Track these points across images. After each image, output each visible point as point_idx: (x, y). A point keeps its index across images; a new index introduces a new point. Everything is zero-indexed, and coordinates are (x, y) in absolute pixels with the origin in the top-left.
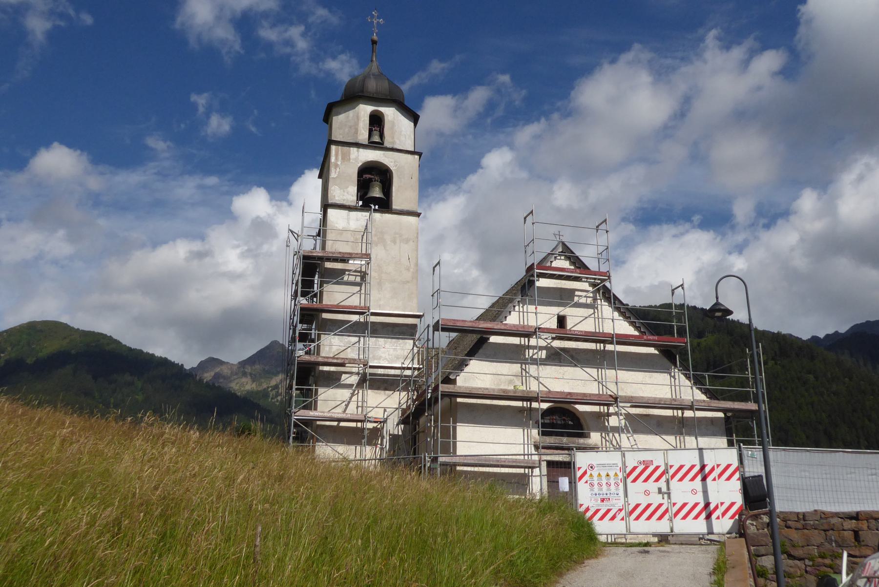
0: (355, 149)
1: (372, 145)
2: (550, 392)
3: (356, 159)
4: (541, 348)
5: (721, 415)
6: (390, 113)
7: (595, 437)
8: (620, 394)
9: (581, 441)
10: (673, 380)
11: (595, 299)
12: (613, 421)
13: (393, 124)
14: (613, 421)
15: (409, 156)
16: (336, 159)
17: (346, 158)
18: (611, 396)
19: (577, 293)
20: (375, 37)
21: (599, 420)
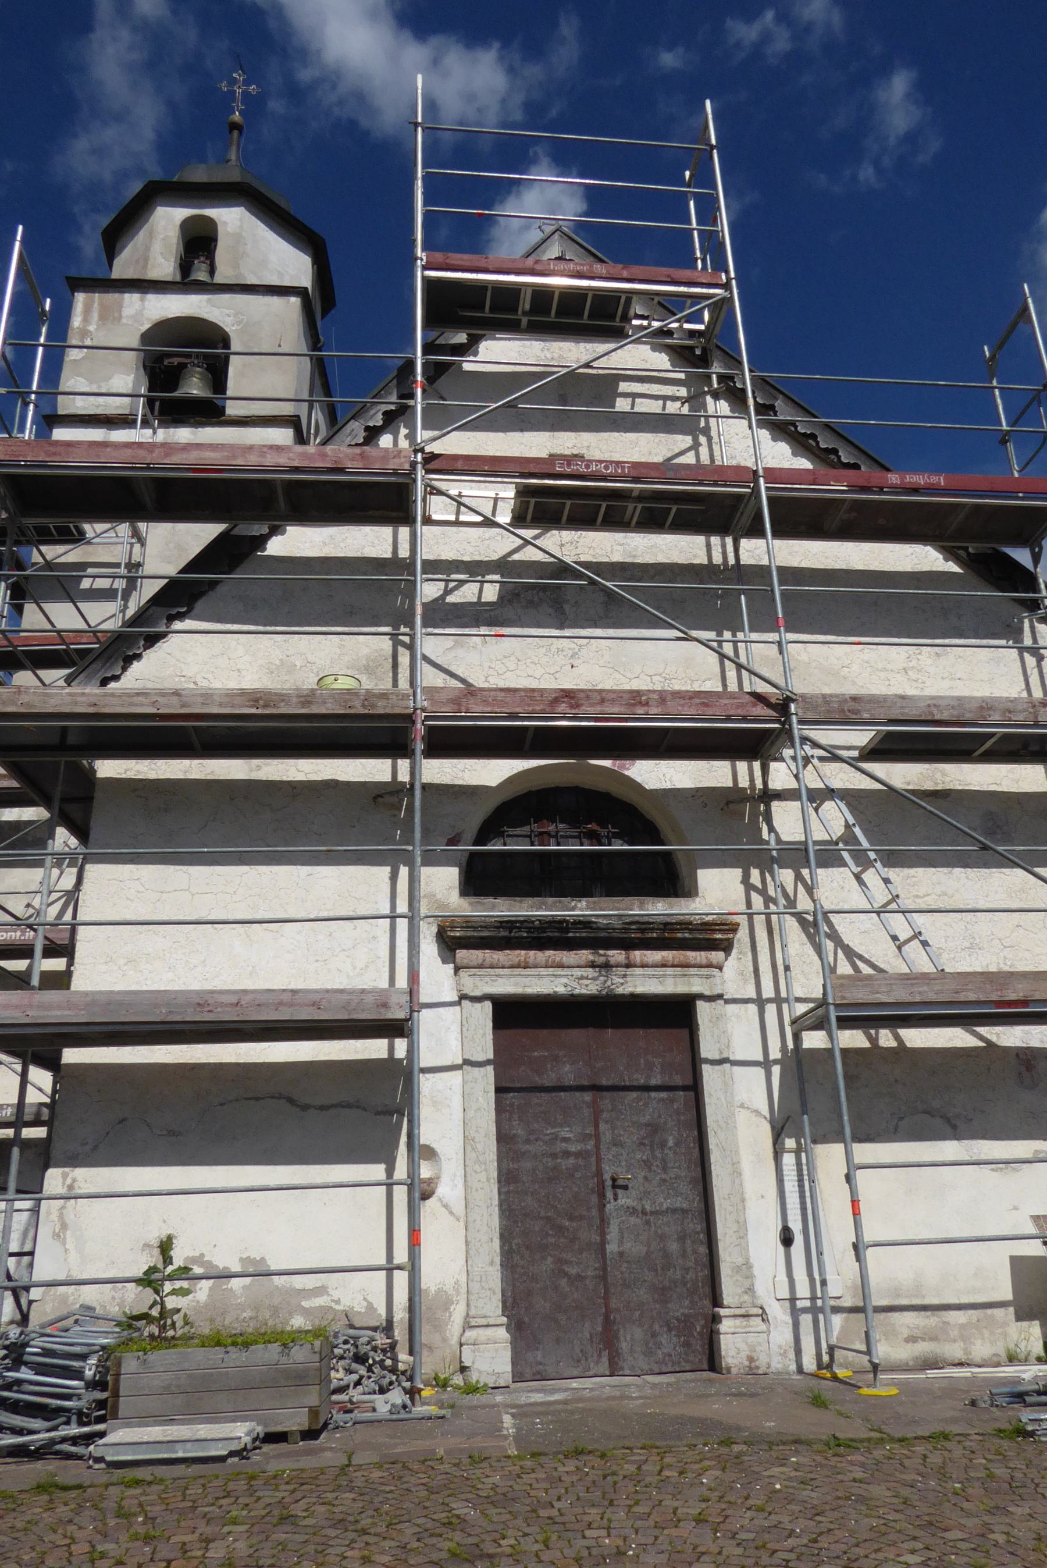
0: (136, 296)
1: (185, 283)
2: (470, 690)
3: (137, 317)
4: (476, 569)
5: (894, 1391)
6: (232, 220)
7: (717, 890)
8: (799, 687)
9: (658, 908)
10: (1030, 661)
11: (695, 400)
12: (788, 822)
13: (238, 238)
14: (788, 822)
15: (275, 301)
16: (86, 320)
17: (109, 316)
18: (759, 698)
19: (624, 387)
20: (237, 117)
21: (736, 814)
